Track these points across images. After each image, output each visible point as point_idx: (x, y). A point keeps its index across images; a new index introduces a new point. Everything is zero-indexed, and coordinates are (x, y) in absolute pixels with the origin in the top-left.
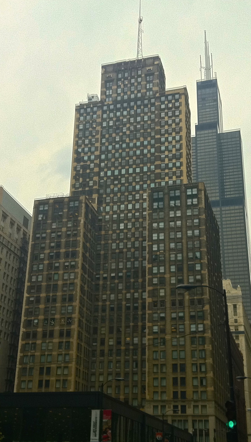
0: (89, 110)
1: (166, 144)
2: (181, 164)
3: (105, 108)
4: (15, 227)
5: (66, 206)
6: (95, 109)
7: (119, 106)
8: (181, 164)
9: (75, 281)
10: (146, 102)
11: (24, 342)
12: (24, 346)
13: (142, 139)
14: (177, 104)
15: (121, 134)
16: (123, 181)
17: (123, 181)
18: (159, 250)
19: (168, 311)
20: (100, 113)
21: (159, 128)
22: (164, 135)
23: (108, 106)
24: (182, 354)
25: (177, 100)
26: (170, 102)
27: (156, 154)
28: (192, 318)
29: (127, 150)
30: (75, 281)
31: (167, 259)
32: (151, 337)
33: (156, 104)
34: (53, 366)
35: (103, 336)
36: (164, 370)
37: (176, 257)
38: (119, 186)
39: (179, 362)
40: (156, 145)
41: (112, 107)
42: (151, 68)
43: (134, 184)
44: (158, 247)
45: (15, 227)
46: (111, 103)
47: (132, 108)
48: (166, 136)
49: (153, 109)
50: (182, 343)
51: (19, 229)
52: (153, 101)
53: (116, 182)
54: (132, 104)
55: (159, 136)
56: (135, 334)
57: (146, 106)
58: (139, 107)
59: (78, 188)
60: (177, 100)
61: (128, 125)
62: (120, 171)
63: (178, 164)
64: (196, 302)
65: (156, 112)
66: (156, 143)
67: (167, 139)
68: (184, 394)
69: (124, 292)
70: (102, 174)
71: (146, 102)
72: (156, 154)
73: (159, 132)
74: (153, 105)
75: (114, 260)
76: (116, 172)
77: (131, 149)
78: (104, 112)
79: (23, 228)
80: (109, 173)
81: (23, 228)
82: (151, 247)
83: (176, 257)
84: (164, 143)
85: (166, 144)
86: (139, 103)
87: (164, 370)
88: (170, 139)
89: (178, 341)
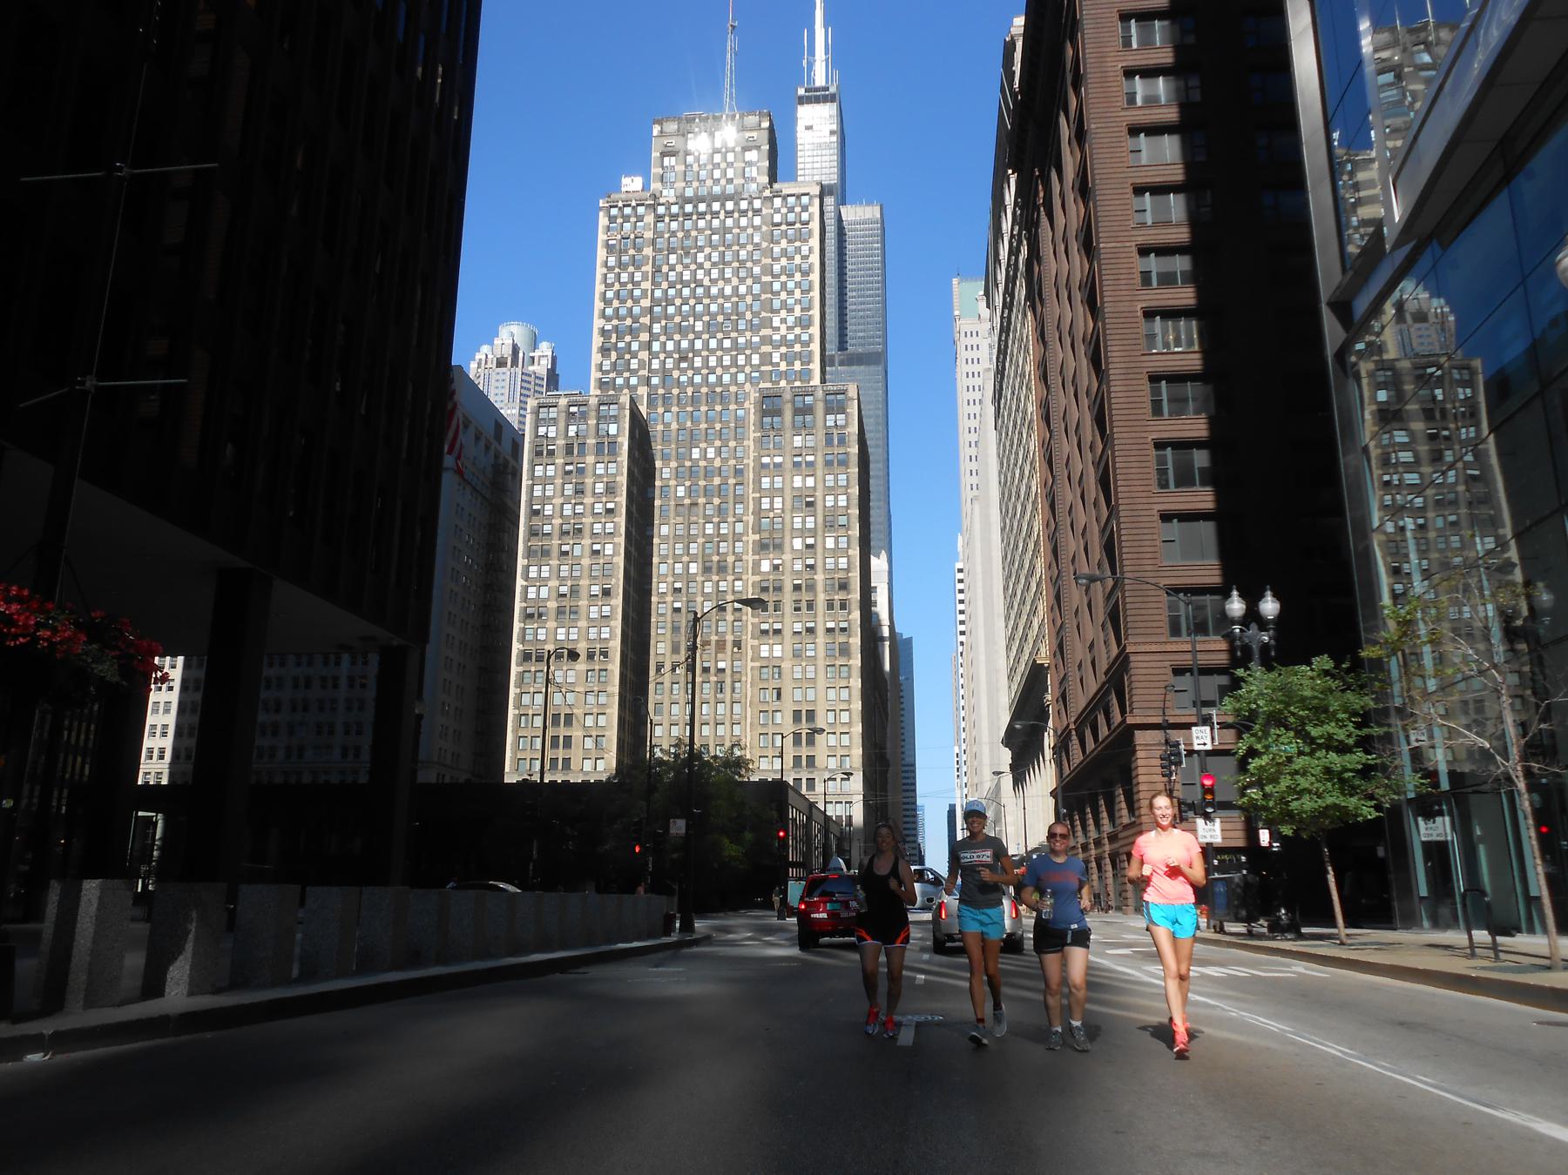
0: (627, 211)
1: (783, 295)
2: (811, 250)
3: (661, 210)
4: (482, 443)
5: (593, 414)
6: (641, 210)
7: (689, 208)
8: (811, 250)
9: (615, 560)
10: (744, 205)
11: (521, 669)
12: (521, 675)
13: (735, 281)
14: (805, 216)
15: (693, 267)
16: (698, 362)
17: (698, 362)
18: (772, 509)
19: (787, 619)
20: (650, 219)
21: (769, 261)
22: (778, 276)
23: (668, 205)
24: (811, 695)
25: (805, 209)
26: (791, 210)
27: (763, 314)
28: (828, 464)
29: (706, 301)
30: (615, 560)
31: (788, 527)
32: (758, 664)
33: (765, 211)
34: (578, 712)
35: (661, 659)
36: (778, 721)
37: (804, 522)
38: (690, 373)
39: (804, 708)
40: (764, 297)
41: (675, 209)
42: (755, 134)
43: (719, 371)
44: (772, 503)
45: (482, 443)
46: (673, 200)
47: (715, 214)
48: (783, 278)
49: (757, 221)
50: (810, 675)
51: (487, 448)
52: (757, 204)
53: (684, 365)
54: (716, 206)
55: (768, 279)
56: (720, 656)
57: (743, 213)
58: (729, 214)
59: (607, 372)
60: (805, 209)
61: (707, 250)
62: (692, 343)
63: (805, 337)
64: (837, 605)
65: (764, 228)
66: (763, 291)
67: (784, 285)
68: (811, 759)
69: (700, 579)
70: (656, 346)
71: (744, 205)
72: (763, 314)
73: (768, 270)
74: (757, 212)
75: (680, 519)
76: (685, 344)
77: (713, 299)
78: (659, 218)
79: (495, 444)
80: (670, 346)
81: (495, 444)
82: (758, 501)
83: (804, 522)
84: (778, 293)
85: (783, 295)
86: (730, 205)
87: (778, 721)
88: (791, 285)
89: (804, 671)
